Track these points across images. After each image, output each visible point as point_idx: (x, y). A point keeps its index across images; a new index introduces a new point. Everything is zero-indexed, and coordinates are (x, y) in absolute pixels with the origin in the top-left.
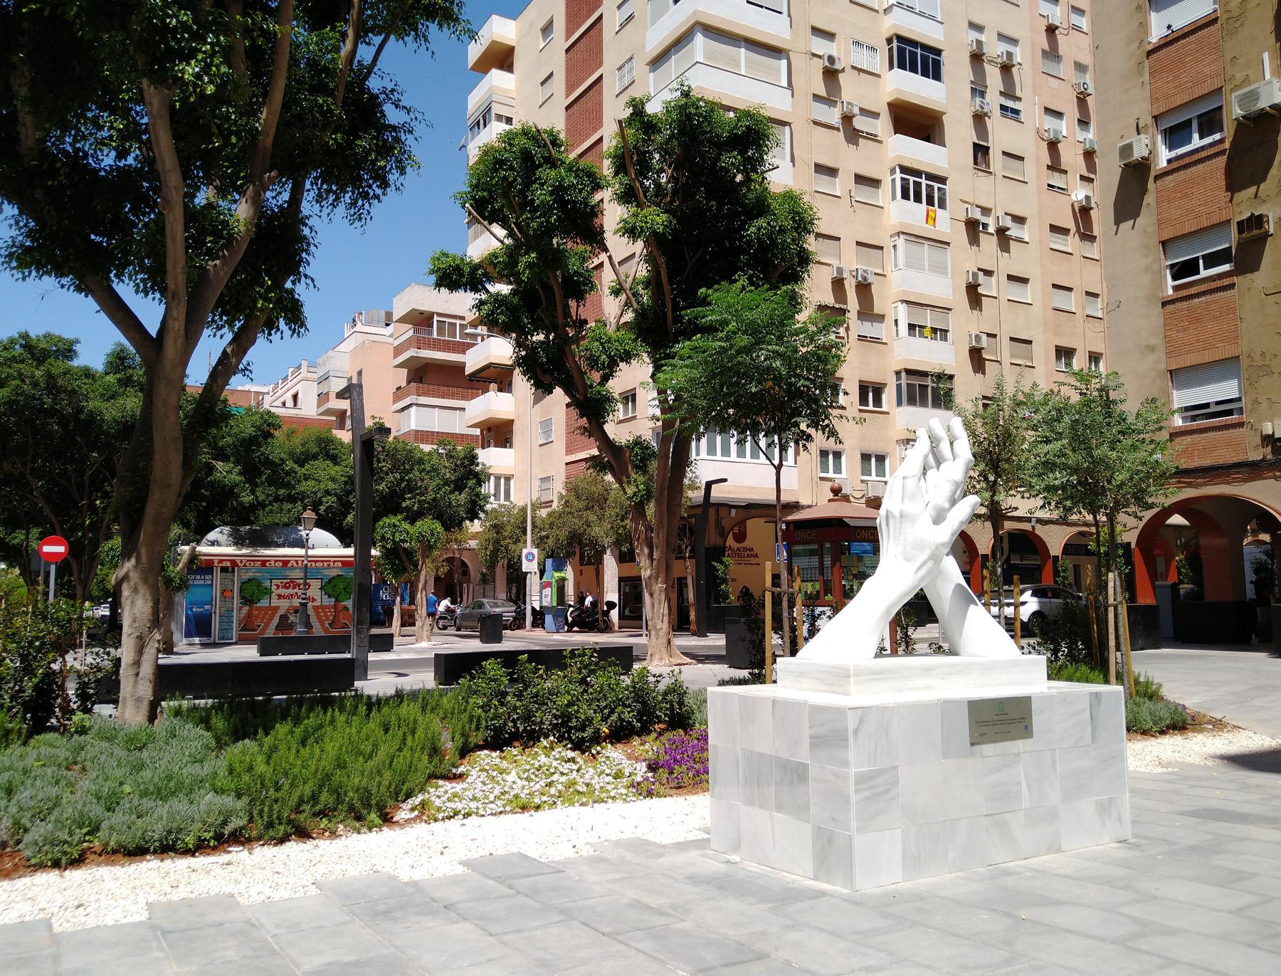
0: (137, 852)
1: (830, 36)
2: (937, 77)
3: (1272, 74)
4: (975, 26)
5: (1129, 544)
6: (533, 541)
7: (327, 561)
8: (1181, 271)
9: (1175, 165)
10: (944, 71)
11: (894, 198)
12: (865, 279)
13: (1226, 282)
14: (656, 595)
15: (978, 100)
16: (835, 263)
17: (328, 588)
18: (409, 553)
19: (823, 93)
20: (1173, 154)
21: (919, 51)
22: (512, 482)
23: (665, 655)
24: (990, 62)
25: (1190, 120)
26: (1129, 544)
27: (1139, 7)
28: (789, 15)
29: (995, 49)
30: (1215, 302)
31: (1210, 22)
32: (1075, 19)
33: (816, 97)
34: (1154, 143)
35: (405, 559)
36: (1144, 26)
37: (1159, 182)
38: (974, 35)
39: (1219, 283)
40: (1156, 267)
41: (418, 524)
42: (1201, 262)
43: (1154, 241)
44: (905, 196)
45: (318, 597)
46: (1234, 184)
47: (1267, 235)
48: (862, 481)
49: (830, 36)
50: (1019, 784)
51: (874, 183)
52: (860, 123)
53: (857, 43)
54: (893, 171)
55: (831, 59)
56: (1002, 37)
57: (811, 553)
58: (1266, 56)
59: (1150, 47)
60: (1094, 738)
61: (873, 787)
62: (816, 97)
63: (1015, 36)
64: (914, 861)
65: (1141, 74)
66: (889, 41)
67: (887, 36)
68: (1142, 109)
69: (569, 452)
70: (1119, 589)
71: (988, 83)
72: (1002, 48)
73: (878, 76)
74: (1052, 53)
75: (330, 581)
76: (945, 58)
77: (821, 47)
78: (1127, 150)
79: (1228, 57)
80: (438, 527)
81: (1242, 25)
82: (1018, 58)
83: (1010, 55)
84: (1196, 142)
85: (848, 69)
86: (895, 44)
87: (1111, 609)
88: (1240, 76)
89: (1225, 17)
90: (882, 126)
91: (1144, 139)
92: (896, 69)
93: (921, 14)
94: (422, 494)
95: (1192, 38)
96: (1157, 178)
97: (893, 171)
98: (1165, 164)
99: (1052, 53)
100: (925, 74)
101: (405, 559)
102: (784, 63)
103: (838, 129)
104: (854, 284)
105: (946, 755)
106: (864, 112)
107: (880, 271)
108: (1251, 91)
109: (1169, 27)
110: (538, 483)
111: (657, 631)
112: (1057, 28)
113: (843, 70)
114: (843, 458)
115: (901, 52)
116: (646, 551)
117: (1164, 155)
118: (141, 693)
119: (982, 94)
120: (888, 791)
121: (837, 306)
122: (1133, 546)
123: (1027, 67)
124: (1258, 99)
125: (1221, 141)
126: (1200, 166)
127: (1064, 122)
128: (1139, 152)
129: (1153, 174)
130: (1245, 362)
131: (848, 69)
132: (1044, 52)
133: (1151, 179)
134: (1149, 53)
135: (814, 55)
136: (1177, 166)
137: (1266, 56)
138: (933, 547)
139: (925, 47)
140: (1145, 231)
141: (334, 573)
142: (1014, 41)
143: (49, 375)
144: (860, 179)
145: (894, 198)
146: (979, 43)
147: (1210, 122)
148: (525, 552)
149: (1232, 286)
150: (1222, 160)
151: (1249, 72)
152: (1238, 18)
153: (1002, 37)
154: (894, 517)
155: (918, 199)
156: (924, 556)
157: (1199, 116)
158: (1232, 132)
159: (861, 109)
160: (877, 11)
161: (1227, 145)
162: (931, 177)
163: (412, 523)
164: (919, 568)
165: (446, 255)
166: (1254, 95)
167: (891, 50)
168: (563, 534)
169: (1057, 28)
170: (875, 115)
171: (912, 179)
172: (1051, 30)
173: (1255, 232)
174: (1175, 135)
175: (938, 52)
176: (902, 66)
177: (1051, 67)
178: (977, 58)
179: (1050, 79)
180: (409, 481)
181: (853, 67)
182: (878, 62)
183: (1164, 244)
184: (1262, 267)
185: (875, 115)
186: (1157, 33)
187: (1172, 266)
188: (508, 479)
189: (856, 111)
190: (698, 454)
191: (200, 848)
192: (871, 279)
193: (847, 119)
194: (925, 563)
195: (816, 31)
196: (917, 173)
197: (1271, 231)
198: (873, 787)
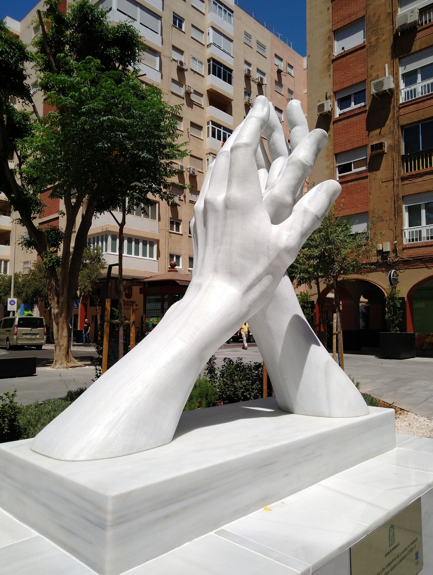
1: (181, 52)
2: (230, 82)
3: (389, 74)
4: (247, 63)
5: (313, 301)
6: (14, 295)
8: (344, 168)
9: (343, 116)
10: (233, 80)
11: (208, 136)
12: (193, 173)
13: (364, 175)
14: (60, 324)
15: (247, 97)
16: (180, 163)
19: (177, 79)
20: (342, 111)
21: (222, 68)
22: (8, 263)
23: (64, 361)
24: (253, 81)
25: (351, 95)
26: (313, 301)
27: (329, 38)
28: (162, 35)
29: (256, 75)
30: (359, 184)
31: (362, 47)
32: (289, 70)
33: (173, 81)
34: (334, 106)
36: (331, 47)
37: (335, 125)
38: (246, 67)
39: (361, 176)
40: (332, 166)
42: (353, 165)
43: (332, 154)
44: (213, 136)
46: (370, 128)
47: (383, 153)
48: (189, 271)
49: (181, 52)
51: (200, 128)
52: (194, 97)
53: (194, 58)
54: (208, 123)
55: (181, 63)
56: (259, 71)
57: (157, 301)
58: (387, 65)
59: (334, 58)
62: (173, 81)
63: (265, 72)
65: (329, 71)
66: (209, 61)
67: (208, 57)
68: (329, 88)
70: (339, 324)
71: (252, 91)
72: (258, 75)
73: (203, 76)
74: (279, 83)
76: (234, 74)
77: (176, 56)
78: (321, 107)
79: (370, 65)
81: (376, 50)
82: (265, 82)
83: (262, 79)
84: (353, 106)
85: (189, 70)
86: (211, 62)
87: (335, 336)
88: (374, 75)
89: (369, 46)
90: (204, 101)
91: (330, 102)
92: (211, 75)
93: (224, 51)
95: (354, 54)
96: (334, 122)
97: (208, 123)
98: (338, 116)
99: (279, 83)
100: (225, 80)
102: (158, 58)
103: (183, 98)
104: (188, 175)
106: (196, 92)
107: (201, 171)
108: (380, 81)
109: (343, 48)
110: (22, 264)
111: (60, 346)
112: (282, 71)
113: (187, 70)
114: (181, 259)
115: (214, 67)
116: (56, 299)
117: (338, 112)
119: (249, 95)
121: (180, 184)
122: (315, 303)
123: (268, 86)
124: (383, 85)
125: (365, 106)
126: (355, 118)
127: (283, 115)
128: (327, 108)
129: (333, 120)
130: (371, 214)
131: (189, 70)
132: (276, 81)
133: (332, 123)
134: (334, 61)
135: (174, 60)
136: (343, 118)
137: (387, 65)
138: (273, 254)
139: (225, 67)
140: (328, 148)
142: (264, 74)
144: (193, 125)
145: (208, 136)
146: (249, 71)
147: (360, 96)
148: (9, 300)
149: (367, 177)
150: (365, 115)
151: (379, 73)
152: (374, 47)
153: (259, 71)
154: (216, 211)
155: (219, 139)
156: (258, 269)
157: (355, 94)
158: (370, 102)
159: (194, 90)
160: (204, 45)
161: (367, 108)
162: (225, 129)
166: (381, 84)
167: (209, 65)
168: (30, 291)
169: (282, 71)
170: (201, 95)
171: (217, 128)
172: (279, 72)
173: (379, 151)
174: (343, 102)
175: (231, 71)
176: (214, 74)
177: (278, 89)
178: (248, 77)
179: (278, 94)
181: (192, 70)
182: (203, 69)
183: (336, 155)
184: (381, 169)
185: (201, 95)
186: (337, 51)
187: (339, 167)
188: (6, 262)
189: (192, 91)
190: (106, 251)
192: (196, 173)
193: (188, 94)
194: (259, 279)
195: (175, 48)
196: (219, 126)
197: (386, 151)
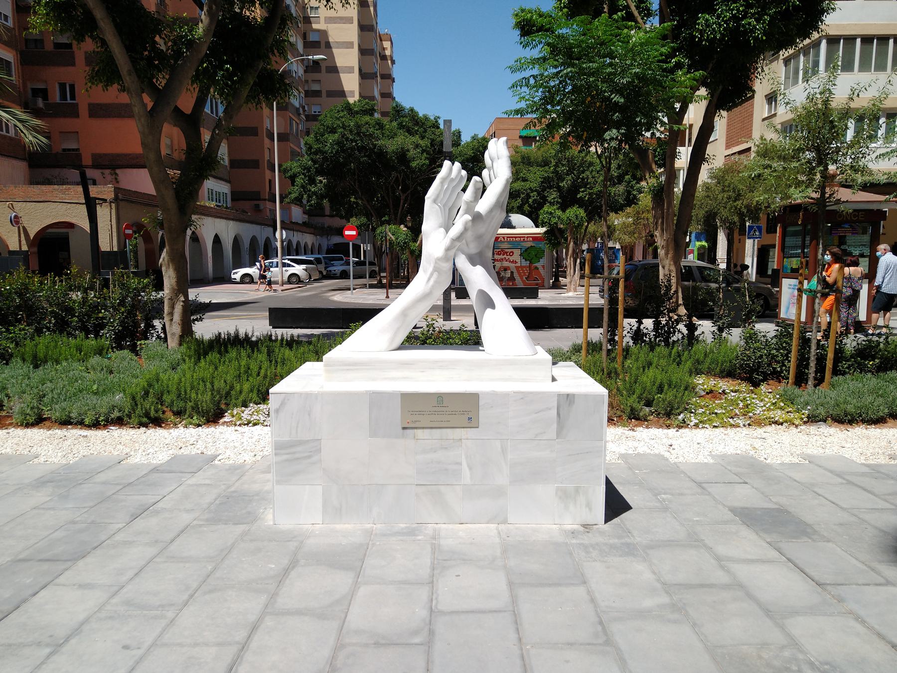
0: (66, 423)
7: (522, 237)
17: (525, 255)
18: (562, 231)
35: (558, 235)
41: (567, 211)
45: (518, 260)
50: (460, 464)
60: (559, 434)
61: (294, 453)
64: (333, 511)
69: (728, 147)
75: (526, 250)
80: (582, 212)
94: (591, 188)
101: (558, 235)
105: (374, 434)
118: (174, 331)
120: (309, 457)
141: (528, 245)
143: (358, 126)
163: (564, 211)
164: (429, 279)
165: (523, 11)
180: (583, 179)
191: (95, 425)
198: (294, 453)
